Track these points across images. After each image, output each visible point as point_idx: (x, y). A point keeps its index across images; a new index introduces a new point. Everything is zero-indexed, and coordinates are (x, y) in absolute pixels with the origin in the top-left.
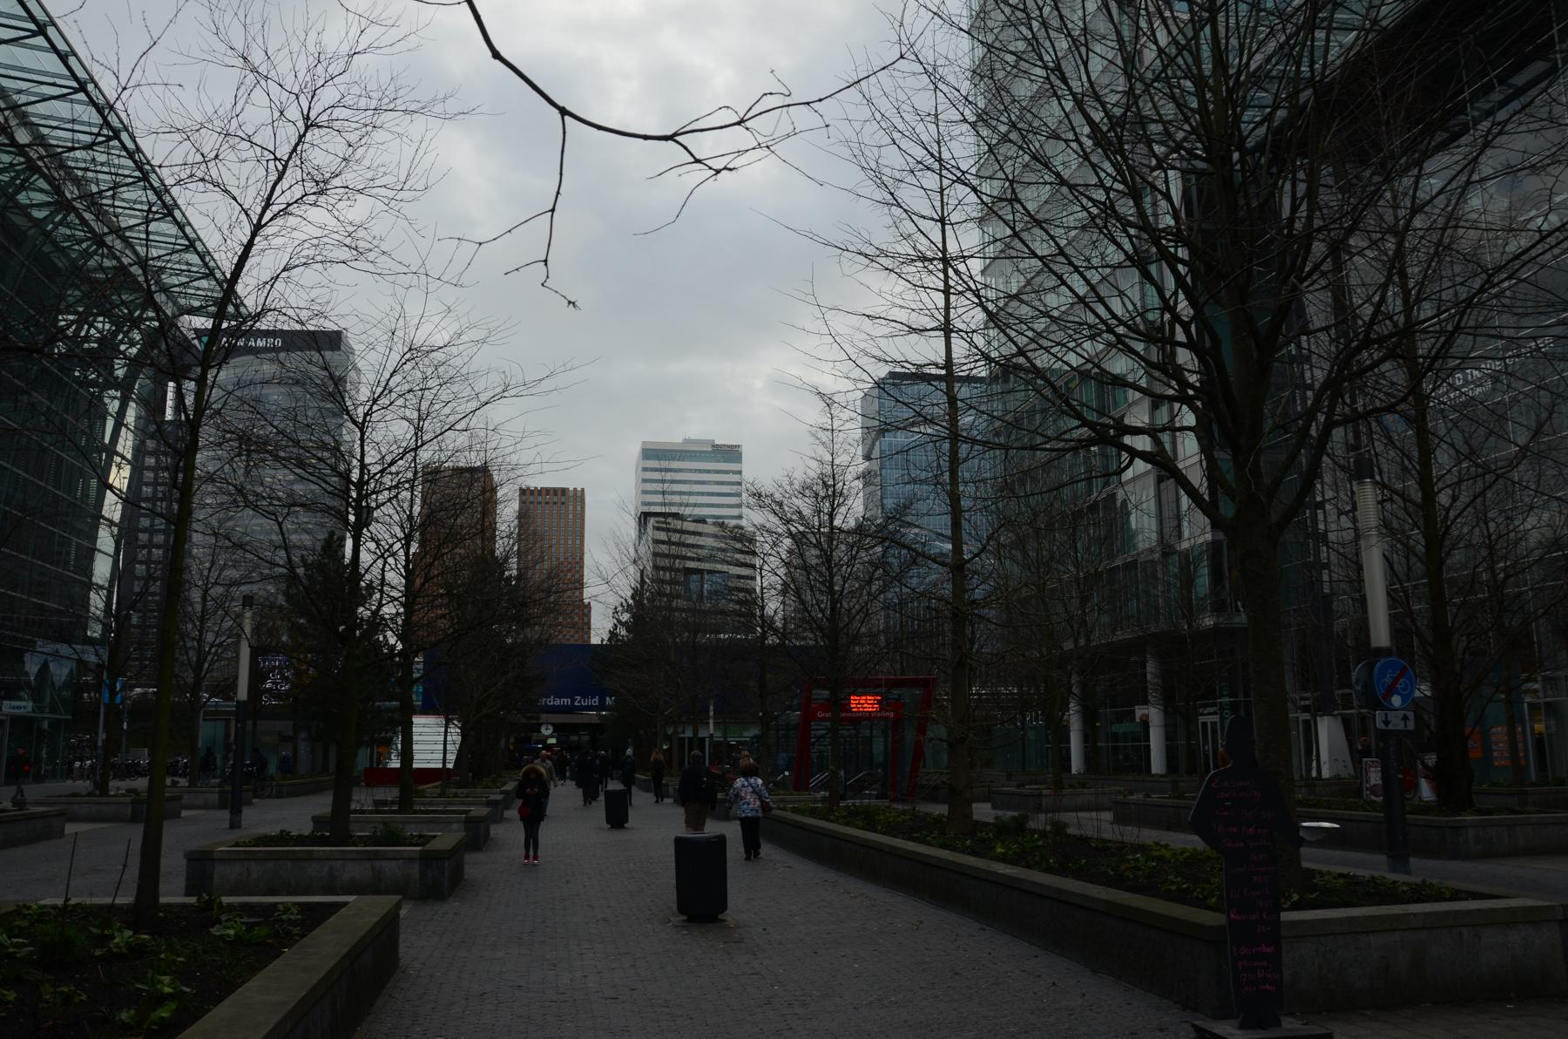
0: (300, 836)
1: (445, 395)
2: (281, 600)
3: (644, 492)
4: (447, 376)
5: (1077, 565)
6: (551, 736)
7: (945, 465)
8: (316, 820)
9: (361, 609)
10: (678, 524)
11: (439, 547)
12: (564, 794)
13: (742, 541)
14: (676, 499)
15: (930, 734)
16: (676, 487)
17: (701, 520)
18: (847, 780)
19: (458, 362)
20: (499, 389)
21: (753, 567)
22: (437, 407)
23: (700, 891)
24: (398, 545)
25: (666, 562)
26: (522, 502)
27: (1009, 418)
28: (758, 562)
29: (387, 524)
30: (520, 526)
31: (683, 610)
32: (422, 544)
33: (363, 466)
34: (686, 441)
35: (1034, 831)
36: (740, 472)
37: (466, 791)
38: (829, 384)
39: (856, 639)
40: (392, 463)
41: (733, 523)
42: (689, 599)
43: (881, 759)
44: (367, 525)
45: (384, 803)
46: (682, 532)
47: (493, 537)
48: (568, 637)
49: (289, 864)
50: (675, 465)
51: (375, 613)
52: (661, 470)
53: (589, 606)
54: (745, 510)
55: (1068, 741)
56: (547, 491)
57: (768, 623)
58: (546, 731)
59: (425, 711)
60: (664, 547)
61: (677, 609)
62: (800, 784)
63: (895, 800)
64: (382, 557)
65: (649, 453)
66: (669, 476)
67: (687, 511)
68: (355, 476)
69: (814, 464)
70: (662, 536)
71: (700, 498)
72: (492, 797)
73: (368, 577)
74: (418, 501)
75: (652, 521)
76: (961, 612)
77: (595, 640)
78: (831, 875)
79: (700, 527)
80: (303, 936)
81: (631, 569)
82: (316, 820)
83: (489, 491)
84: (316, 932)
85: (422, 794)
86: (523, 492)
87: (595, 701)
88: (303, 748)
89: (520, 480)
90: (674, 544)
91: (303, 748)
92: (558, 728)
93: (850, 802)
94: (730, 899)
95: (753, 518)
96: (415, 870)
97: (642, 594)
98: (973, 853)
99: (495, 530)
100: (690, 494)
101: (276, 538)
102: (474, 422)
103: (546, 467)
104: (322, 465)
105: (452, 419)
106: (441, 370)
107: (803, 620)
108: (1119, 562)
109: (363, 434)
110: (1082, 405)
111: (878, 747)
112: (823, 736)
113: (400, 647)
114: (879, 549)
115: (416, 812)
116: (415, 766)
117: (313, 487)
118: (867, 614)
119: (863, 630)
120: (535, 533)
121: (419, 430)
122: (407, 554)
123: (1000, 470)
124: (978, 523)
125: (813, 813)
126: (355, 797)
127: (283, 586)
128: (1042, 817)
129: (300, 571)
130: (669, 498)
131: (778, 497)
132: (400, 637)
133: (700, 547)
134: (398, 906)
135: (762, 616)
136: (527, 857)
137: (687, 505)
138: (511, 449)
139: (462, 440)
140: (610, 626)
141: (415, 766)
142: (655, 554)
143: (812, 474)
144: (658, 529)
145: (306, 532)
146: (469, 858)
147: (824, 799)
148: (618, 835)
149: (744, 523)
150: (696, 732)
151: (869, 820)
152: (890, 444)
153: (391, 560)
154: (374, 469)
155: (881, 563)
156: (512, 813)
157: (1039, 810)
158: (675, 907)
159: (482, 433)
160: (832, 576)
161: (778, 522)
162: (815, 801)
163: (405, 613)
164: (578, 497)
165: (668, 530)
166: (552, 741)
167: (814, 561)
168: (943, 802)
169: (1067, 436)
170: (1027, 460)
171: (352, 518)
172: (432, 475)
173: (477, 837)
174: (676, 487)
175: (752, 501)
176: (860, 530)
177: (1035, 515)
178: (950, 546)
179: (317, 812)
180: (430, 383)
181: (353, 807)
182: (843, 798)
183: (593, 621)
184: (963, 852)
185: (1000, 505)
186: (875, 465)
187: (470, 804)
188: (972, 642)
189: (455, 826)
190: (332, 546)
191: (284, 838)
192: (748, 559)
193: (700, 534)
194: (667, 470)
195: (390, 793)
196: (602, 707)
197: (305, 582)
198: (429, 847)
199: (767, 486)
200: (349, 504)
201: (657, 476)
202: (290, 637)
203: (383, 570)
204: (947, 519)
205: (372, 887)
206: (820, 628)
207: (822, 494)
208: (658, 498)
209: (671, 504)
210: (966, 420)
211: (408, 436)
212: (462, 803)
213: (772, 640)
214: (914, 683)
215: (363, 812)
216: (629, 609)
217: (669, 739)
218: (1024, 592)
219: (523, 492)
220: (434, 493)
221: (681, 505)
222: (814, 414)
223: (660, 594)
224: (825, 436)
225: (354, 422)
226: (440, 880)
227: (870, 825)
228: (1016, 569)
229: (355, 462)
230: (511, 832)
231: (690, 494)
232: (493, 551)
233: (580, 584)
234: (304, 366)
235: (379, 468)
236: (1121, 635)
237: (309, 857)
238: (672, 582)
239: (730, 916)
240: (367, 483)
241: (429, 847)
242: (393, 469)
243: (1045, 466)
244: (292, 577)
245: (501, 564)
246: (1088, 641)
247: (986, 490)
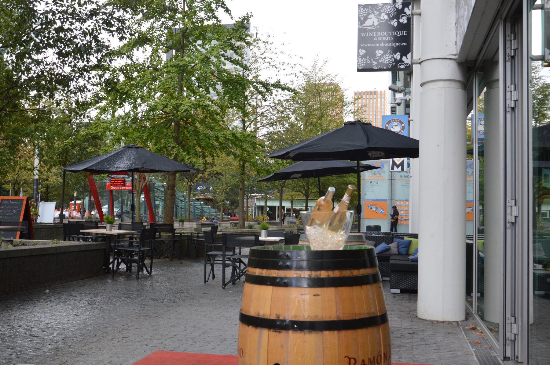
216: (44, 294)
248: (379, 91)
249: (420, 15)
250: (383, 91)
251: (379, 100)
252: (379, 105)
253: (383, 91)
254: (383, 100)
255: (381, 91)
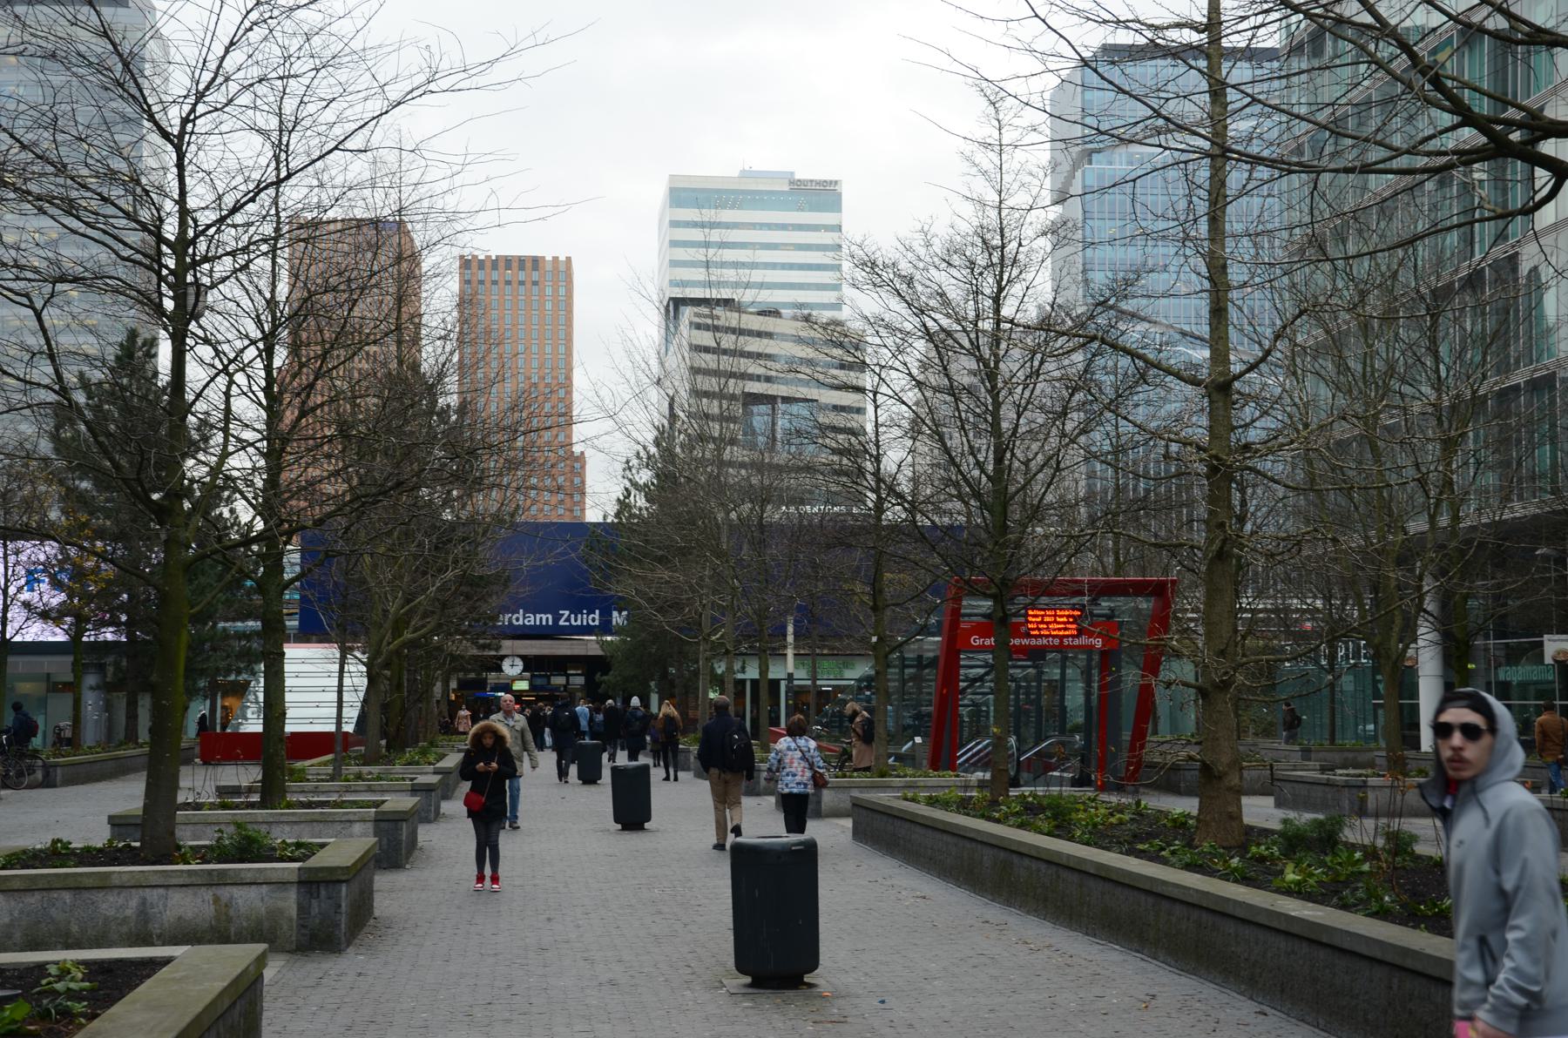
0: (87, 850)
1: (325, 85)
2: (45, 447)
3: (674, 264)
4: (328, 54)
5: (1438, 384)
6: (520, 678)
7: (1202, 207)
8: (116, 823)
9: (190, 462)
10: (727, 318)
11: (324, 357)
12: (538, 775)
13: (845, 348)
14: (730, 274)
15: (1164, 675)
16: (729, 255)
17: (772, 312)
18: (1021, 752)
19: (344, 27)
20: (421, 78)
21: (860, 390)
22: (311, 108)
23: (775, 928)
24: (251, 352)
25: (710, 384)
26: (465, 282)
27: (1322, 117)
28: (868, 381)
29: (233, 310)
30: (463, 321)
31: (742, 465)
32: (295, 349)
33: (184, 213)
34: (746, 174)
35: (1352, 847)
36: (839, 228)
37: (375, 769)
38: (997, 65)
39: (1036, 513)
40: (236, 209)
41: (825, 316)
42: (753, 446)
43: (1080, 720)
44: (196, 316)
45: (236, 791)
46: (740, 332)
47: (416, 340)
48: (543, 509)
49: (67, 896)
50: (727, 215)
51: (215, 471)
52: (702, 225)
53: (581, 458)
54: (848, 291)
55: (1414, 694)
56: (508, 261)
57: (886, 487)
58: (512, 668)
59: (311, 632)
60: (708, 357)
61: (730, 464)
62: (942, 759)
63: (1103, 788)
64: (224, 380)
65: (682, 195)
66: (715, 235)
67: (746, 296)
68: (170, 230)
69: (968, 210)
70: (706, 339)
71: (769, 272)
72: (421, 779)
73: (200, 406)
74: (284, 275)
75: (687, 313)
76: (1224, 468)
77: (593, 516)
78: (994, 912)
79: (768, 324)
80: (94, 1017)
81: (654, 394)
82: (116, 823)
83: (407, 259)
84: (116, 1009)
85: (301, 776)
86: (466, 263)
87: (595, 619)
88: (91, 702)
89: (463, 239)
90: (725, 352)
91: (91, 702)
92: (531, 663)
93: (1027, 790)
94: (822, 949)
95: (862, 305)
96: (289, 902)
97: (672, 438)
98: (1245, 880)
99: (418, 326)
100: (754, 266)
101: (36, 341)
102: (380, 135)
103: (506, 216)
104: (110, 210)
105: (338, 131)
106: (316, 41)
107: (948, 482)
108: (1519, 377)
109: (181, 156)
110: (1466, 85)
111: (1075, 698)
112: (981, 679)
113: (259, 525)
114: (1078, 357)
115: (290, 806)
116: (289, 729)
117: (95, 249)
118: (1058, 469)
119: (1049, 498)
120: (488, 332)
121: (281, 150)
122: (268, 368)
123: (1299, 215)
124: (1257, 309)
125: (964, 806)
126: (184, 783)
127: (49, 424)
128: (1369, 823)
129: (80, 398)
130: (716, 274)
131: (905, 268)
132: (260, 510)
133: (769, 357)
134: (261, 961)
135: (876, 474)
136: (481, 879)
137: (748, 285)
138: (445, 185)
139: (359, 168)
140: (618, 493)
141: (289, 729)
142: (695, 371)
143: (965, 228)
144: (698, 327)
145: (89, 330)
146: (383, 881)
147: (982, 785)
148: (633, 840)
149: (845, 314)
150: (764, 671)
151: (1061, 821)
152: (1101, 177)
153: (240, 378)
154: (206, 218)
155: (1082, 382)
156: (455, 807)
157: (1362, 812)
158: (731, 961)
159: (391, 157)
160: (997, 405)
161: (906, 312)
162: (966, 787)
163: (269, 469)
164: (562, 272)
165: (716, 329)
166: (522, 685)
167: (967, 380)
168: (1189, 793)
169: (1433, 145)
170: (1348, 192)
171: (169, 305)
172: (309, 231)
173: (395, 847)
174: (729, 255)
175: (860, 275)
176: (1045, 325)
177: (1363, 295)
178: (1207, 353)
179: (120, 808)
180: (297, 67)
181: (181, 799)
182: (1015, 783)
183: (589, 482)
184: (1225, 877)
185: (1298, 278)
186: (1074, 208)
187: (383, 791)
188: (1242, 520)
189: (357, 828)
190: (134, 354)
191: (58, 853)
192: (851, 377)
193: (769, 335)
194: (713, 225)
195: (247, 775)
196: (605, 627)
197: (88, 414)
198: (313, 862)
199: (885, 247)
200: (161, 278)
201: (697, 235)
202: (64, 512)
203: (227, 394)
204: (1203, 305)
205: (219, 932)
206: (977, 495)
207: (981, 261)
208: (699, 274)
209: (719, 284)
210: (1239, 127)
211: (263, 161)
212: (370, 790)
213: (895, 513)
214: (1139, 589)
215: (198, 806)
216: (650, 462)
217: (719, 682)
218: (1342, 431)
219: (466, 263)
220: (313, 260)
221: (736, 285)
222: (972, 118)
223: (702, 438)
224: (987, 160)
225: (166, 135)
226: (331, 917)
227: (1062, 828)
228: (1325, 392)
229: (169, 206)
230: (450, 835)
231: (754, 266)
232: (415, 367)
233: (565, 420)
234: (62, 29)
235: (213, 216)
236: (1518, 510)
237: (104, 885)
238: (723, 418)
239: (823, 977)
240: (193, 242)
241: (313, 862)
242: (239, 218)
243: (1384, 205)
244: (65, 411)
245: (431, 389)
246: (1456, 518)
247: (1276, 250)
248: (549, 258)
249: (667, 779)
250: (562, 258)
251: (549, 291)
252: (549, 306)
253: (562, 258)
254: (562, 291)
255: (555, 259)
